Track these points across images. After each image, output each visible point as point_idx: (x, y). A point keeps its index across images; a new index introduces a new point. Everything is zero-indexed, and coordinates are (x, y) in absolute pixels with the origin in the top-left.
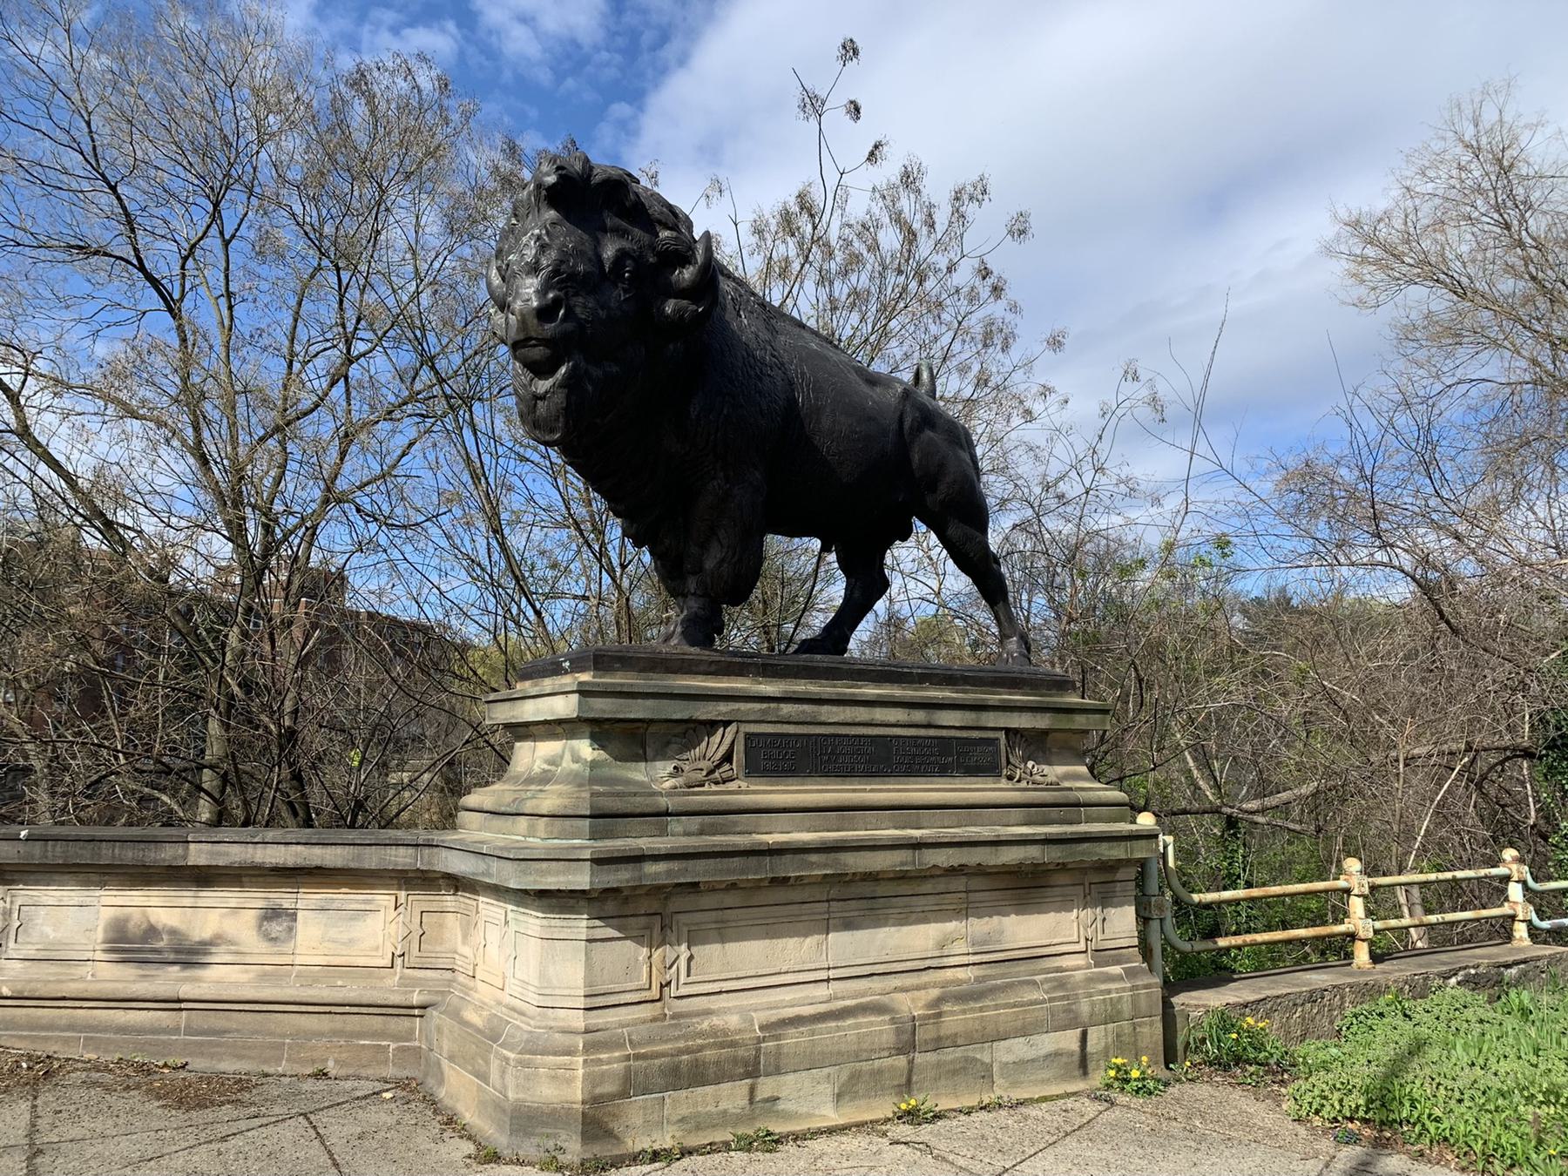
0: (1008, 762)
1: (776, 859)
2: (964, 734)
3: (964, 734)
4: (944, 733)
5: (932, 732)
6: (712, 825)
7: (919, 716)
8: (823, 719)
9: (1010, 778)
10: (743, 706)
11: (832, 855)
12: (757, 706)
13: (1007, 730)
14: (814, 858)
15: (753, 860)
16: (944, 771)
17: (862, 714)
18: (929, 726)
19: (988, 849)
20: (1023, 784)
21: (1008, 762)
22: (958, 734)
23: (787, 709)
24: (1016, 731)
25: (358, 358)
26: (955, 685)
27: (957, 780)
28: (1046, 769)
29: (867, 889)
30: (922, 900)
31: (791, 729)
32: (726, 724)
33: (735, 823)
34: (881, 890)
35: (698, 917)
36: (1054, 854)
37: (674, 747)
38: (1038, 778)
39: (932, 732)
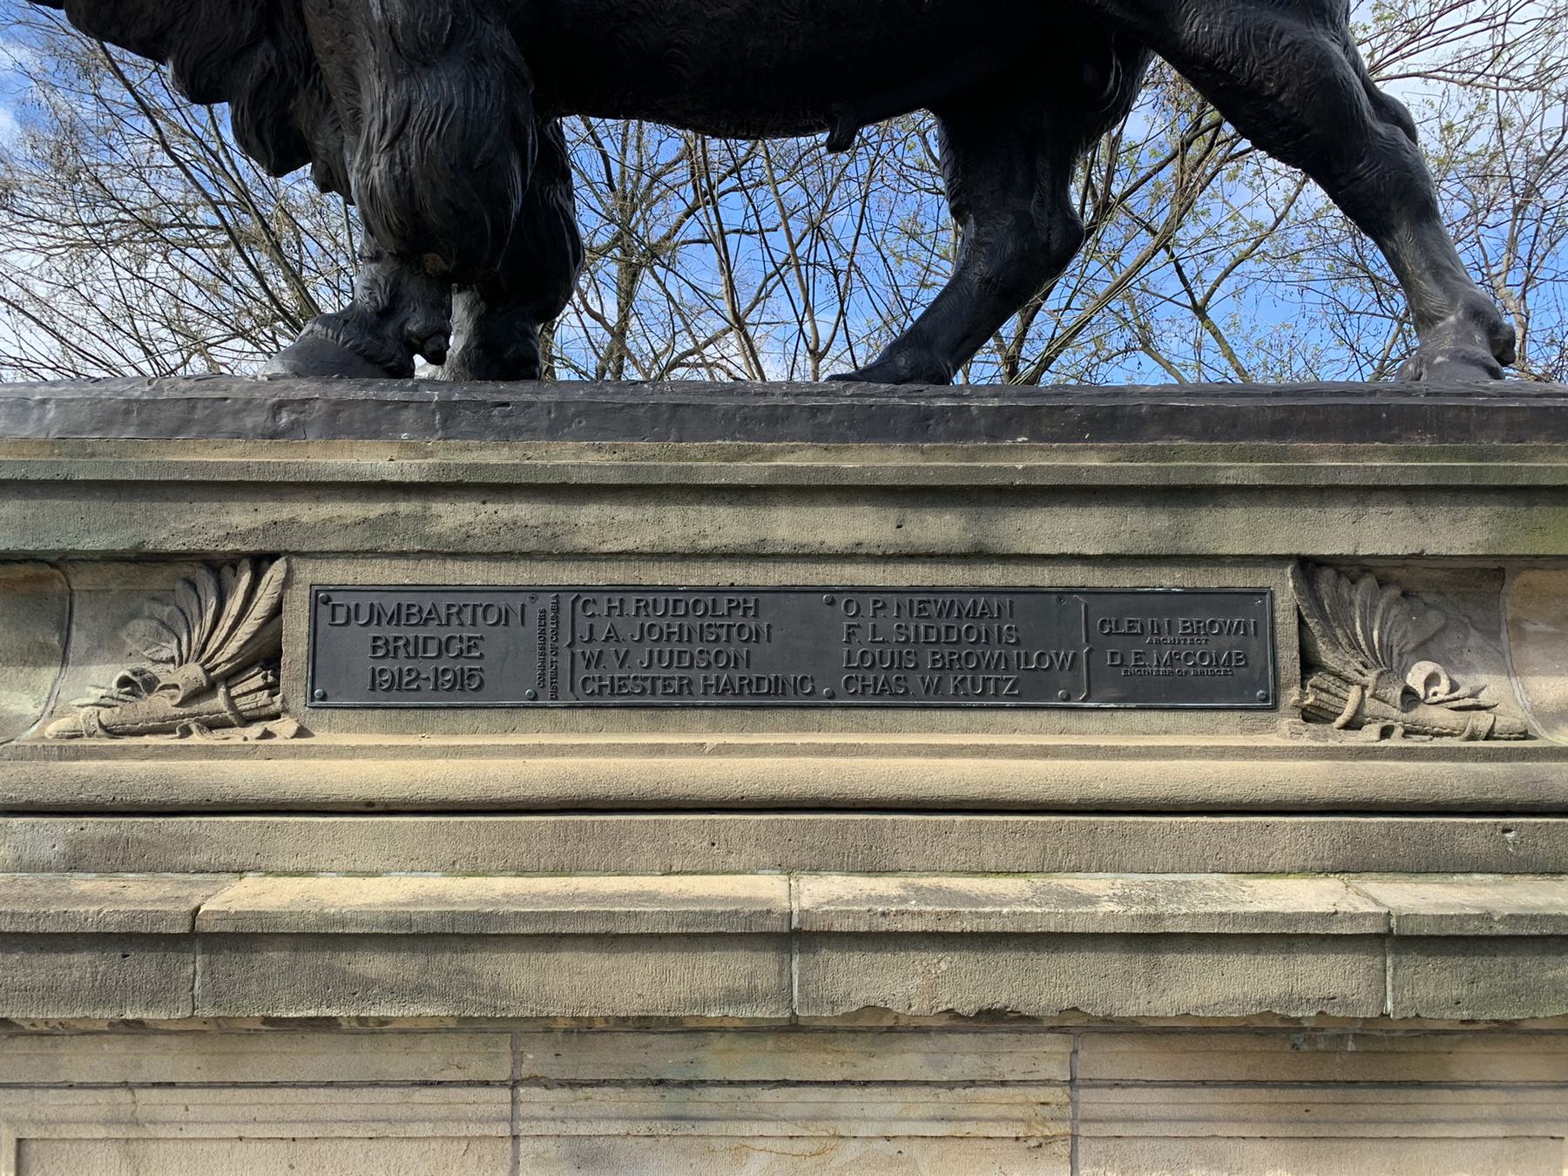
0: (1309, 664)
1: (230, 964)
2: (1124, 579)
3: (1124, 579)
4: (1043, 577)
5: (991, 576)
6: (112, 843)
7: (941, 527)
8: (582, 542)
9: (1313, 715)
10: (307, 512)
11: (446, 960)
12: (352, 510)
13: (1308, 567)
14: (375, 965)
15: (144, 967)
16: (1032, 689)
17: (727, 525)
18: (977, 556)
19: (1115, 962)
20: (1369, 735)
21: (1309, 664)
22: (1098, 578)
23: (452, 516)
24: (1350, 568)
25: (730, 173)
26: (1129, 435)
27: (1094, 721)
28: (1492, 686)
29: (667, 1057)
30: (893, 1103)
31: (475, 574)
32: (260, 562)
33: (187, 842)
34: (715, 1061)
35: (52, 1103)
36: (1430, 989)
37: (140, 626)
38: (1440, 716)
39: (991, 576)
